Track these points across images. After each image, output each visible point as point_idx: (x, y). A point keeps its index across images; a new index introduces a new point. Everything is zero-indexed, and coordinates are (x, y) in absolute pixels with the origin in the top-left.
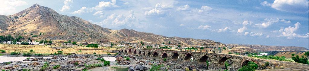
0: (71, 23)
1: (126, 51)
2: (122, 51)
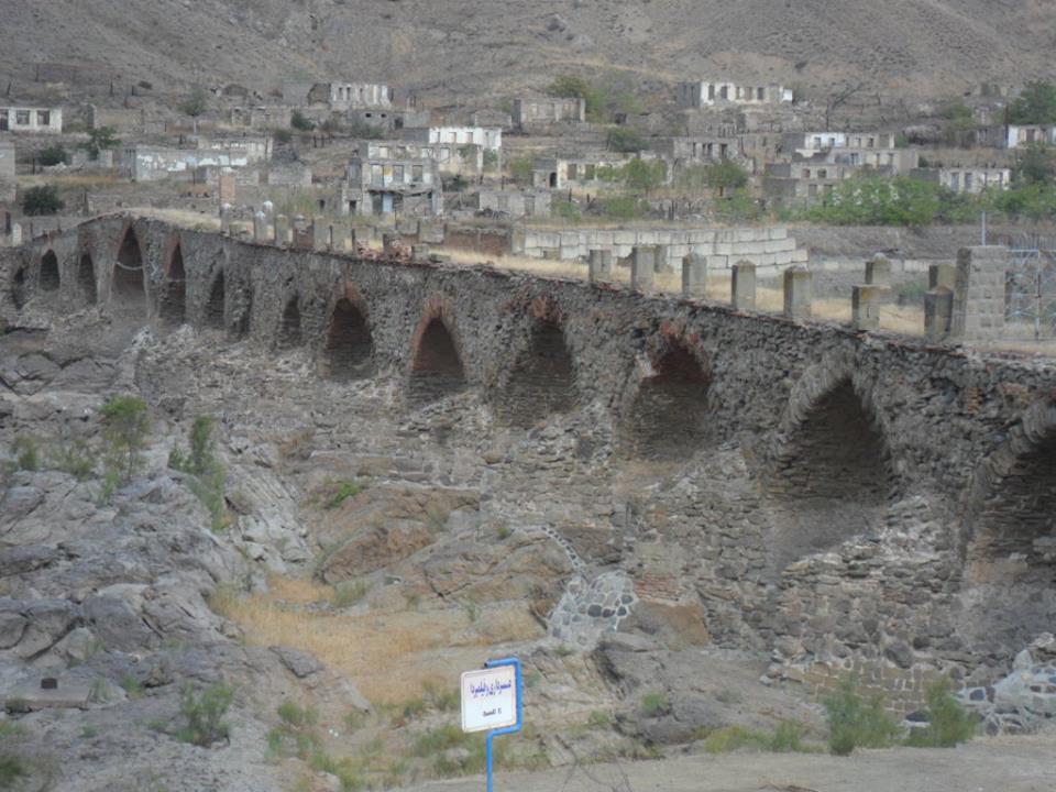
1: (86, 262)
2: (50, 261)
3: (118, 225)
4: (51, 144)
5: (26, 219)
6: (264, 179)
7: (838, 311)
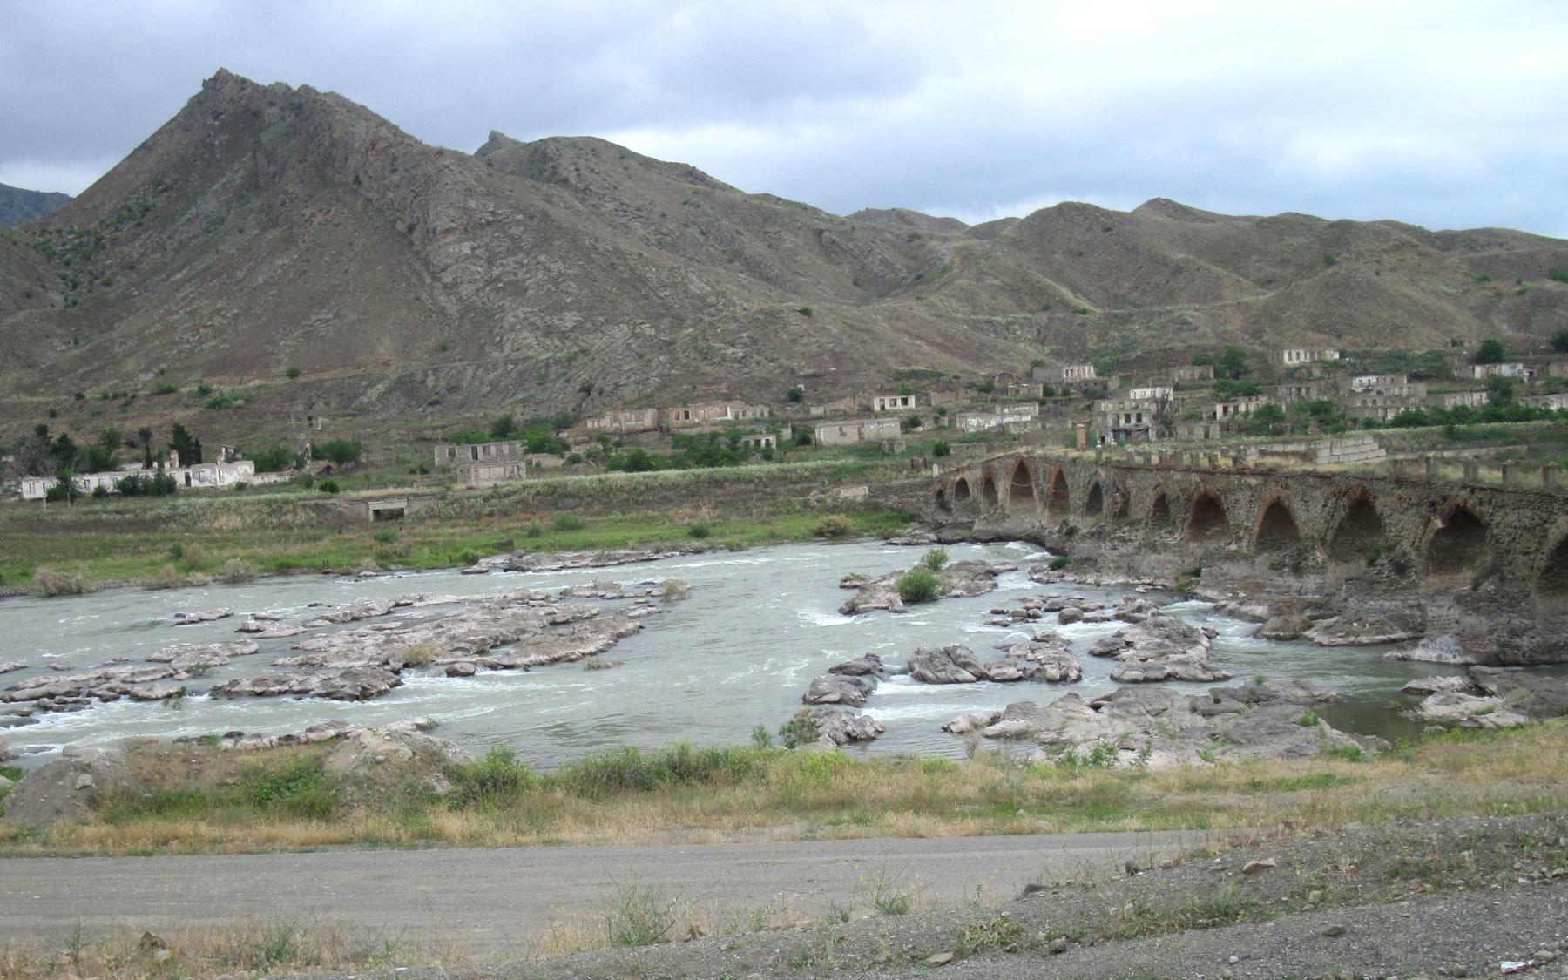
0: (515, 231)
1: (989, 484)
2: (962, 486)
3: (1013, 461)
4: (911, 415)
5: (938, 460)
6: (1043, 426)
7: (259, 388)
